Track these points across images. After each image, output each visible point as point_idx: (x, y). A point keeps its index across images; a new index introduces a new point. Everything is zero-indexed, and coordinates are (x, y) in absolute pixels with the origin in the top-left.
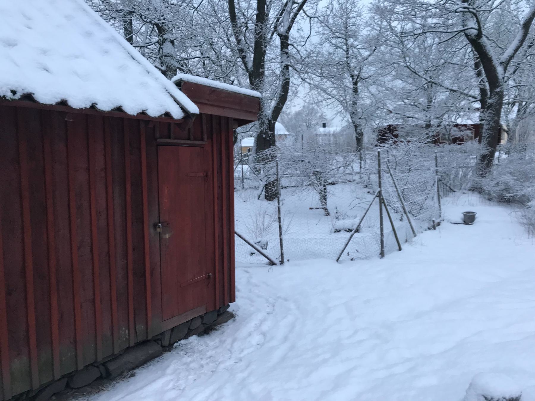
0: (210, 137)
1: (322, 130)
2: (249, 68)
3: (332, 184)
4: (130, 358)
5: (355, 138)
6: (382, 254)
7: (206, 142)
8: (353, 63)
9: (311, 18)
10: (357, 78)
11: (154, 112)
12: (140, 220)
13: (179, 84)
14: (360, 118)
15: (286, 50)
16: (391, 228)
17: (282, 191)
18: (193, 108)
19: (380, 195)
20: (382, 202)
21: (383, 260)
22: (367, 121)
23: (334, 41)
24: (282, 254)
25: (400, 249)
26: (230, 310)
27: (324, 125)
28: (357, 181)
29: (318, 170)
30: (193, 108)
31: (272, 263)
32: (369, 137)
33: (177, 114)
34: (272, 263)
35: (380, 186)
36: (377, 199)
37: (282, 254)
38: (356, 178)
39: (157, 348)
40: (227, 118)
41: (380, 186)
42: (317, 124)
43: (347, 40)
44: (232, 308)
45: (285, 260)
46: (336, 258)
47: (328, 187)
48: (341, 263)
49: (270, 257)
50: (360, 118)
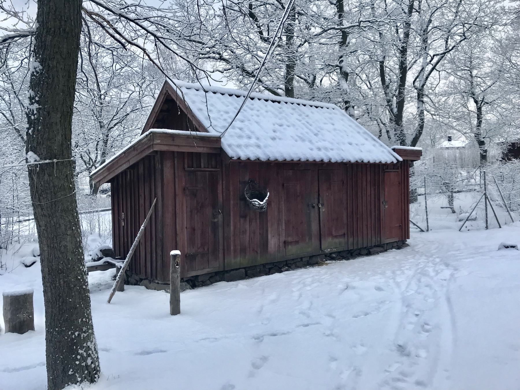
0: (401, 168)
1: (446, 144)
2: (394, 112)
3: (458, 192)
4: (375, 249)
5: (479, 155)
6: (487, 228)
7: (399, 170)
8: (477, 91)
9: (439, 72)
10: (482, 103)
11: (389, 162)
12: (379, 200)
13: (394, 150)
14: (484, 138)
15: (422, 99)
16: (494, 215)
17: (419, 197)
18: (401, 159)
19: (485, 194)
20: (486, 198)
21: (487, 231)
22: (491, 139)
23: (459, 74)
24: (428, 226)
25: (500, 227)
26: (406, 243)
27: (450, 139)
28: (477, 190)
29: (447, 182)
30: (401, 159)
31: (422, 231)
32: (494, 151)
33: (395, 161)
34: (422, 231)
35: (485, 190)
36: (484, 196)
37: (428, 226)
38: (477, 188)
39: (382, 249)
40: (407, 160)
41: (485, 190)
42: (442, 137)
43: (471, 73)
44: (408, 241)
45: (429, 229)
46: (459, 229)
47: (454, 195)
48: (462, 231)
49: (421, 227)
50: (484, 138)
